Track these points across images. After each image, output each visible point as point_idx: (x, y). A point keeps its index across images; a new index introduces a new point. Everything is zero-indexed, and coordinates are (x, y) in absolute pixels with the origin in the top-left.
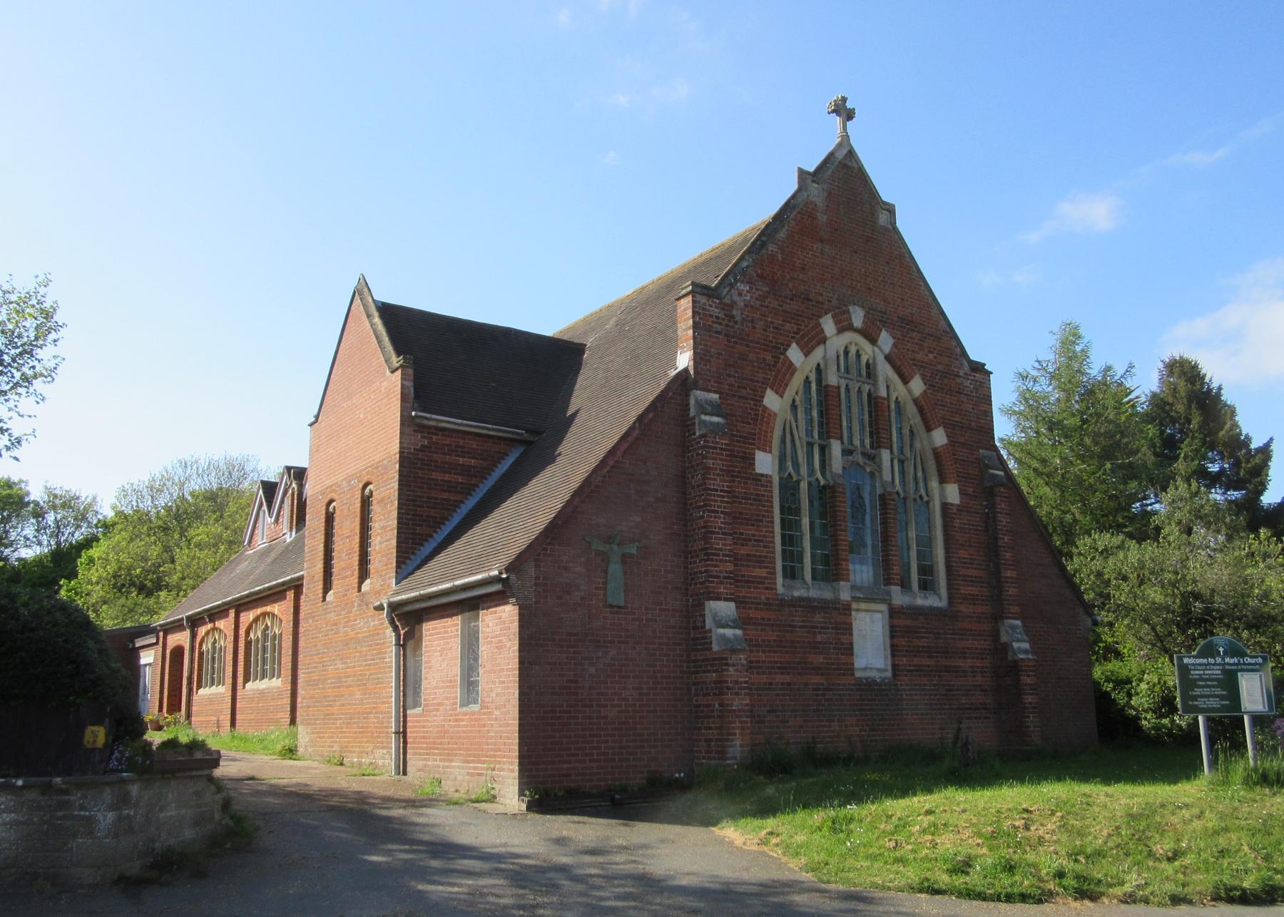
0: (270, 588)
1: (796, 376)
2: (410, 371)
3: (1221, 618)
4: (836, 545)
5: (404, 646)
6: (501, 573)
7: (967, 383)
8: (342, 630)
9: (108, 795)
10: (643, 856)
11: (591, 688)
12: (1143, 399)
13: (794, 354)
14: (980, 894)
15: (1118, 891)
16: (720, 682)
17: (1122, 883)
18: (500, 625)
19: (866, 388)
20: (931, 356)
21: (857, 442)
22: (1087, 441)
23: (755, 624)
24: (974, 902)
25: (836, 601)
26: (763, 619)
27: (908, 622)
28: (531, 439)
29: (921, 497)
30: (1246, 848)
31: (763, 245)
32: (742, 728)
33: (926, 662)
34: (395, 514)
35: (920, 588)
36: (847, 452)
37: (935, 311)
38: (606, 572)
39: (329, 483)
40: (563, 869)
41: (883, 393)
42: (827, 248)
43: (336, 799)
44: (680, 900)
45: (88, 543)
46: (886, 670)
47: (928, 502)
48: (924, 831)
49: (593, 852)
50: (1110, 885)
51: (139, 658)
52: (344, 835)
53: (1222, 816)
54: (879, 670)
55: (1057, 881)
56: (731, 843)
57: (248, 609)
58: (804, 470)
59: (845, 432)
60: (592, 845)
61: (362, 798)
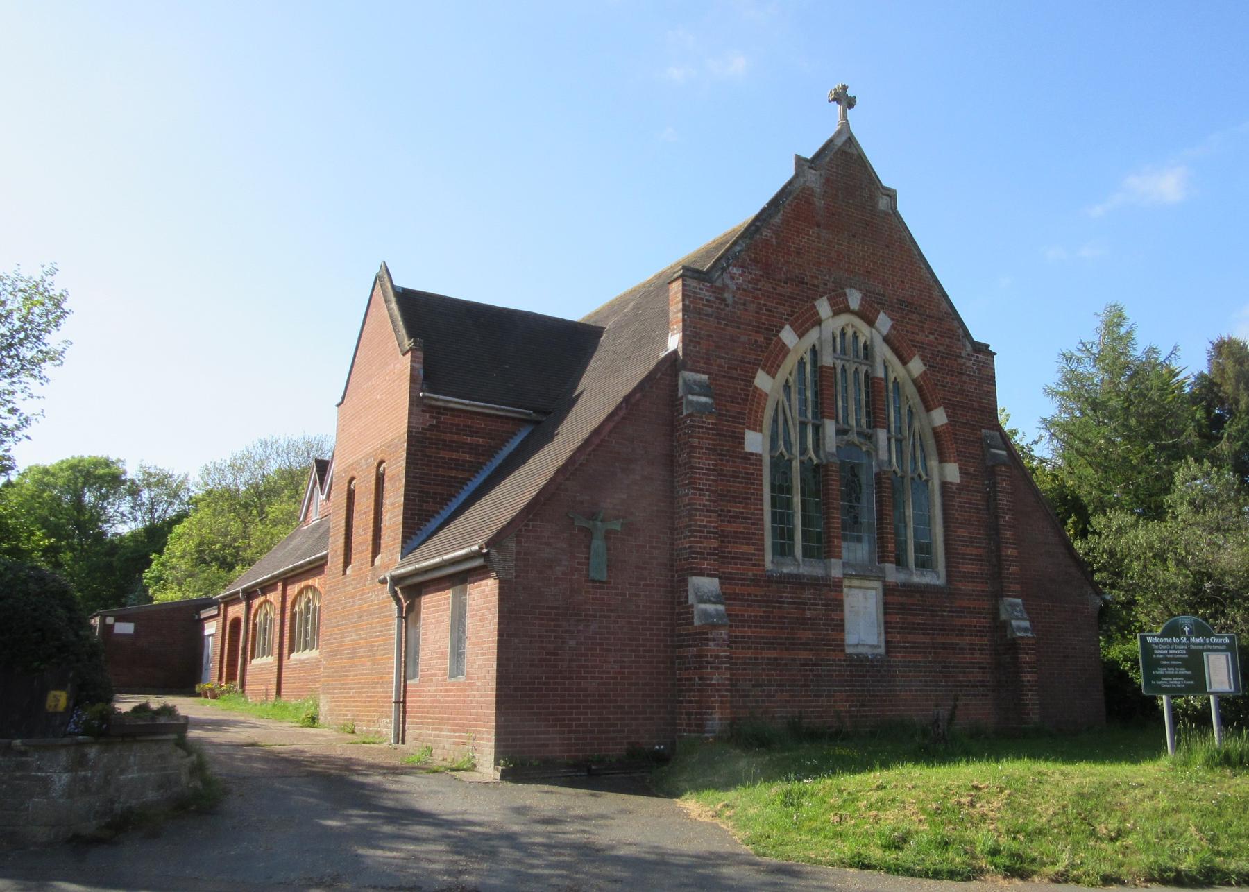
0: (310, 563)
1: (789, 357)
2: (420, 354)
3: (1232, 598)
4: (828, 523)
5: (406, 618)
6: (481, 548)
7: (970, 364)
8: (358, 603)
9: (63, 757)
10: (595, 826)
11: (571, 660)
12: (1192, 380)
13: (788, 336)
14: (908, 870)
15: (1050, 870)
16: (701, 656)
17: (1054, 863)
18: (483, 596)
19: (863, 369)
20: (931, 337)
21: (853, 422)
22: (1133, 422)
23: (741, 600)
24: (901, 878)
25: (827, 577)
26: (749, 595)
27: (903, 600)
28: (540, 418)
29: (920, 476)
30: (1193, 829)
31: (758, 230)
32: (721, 702)
33: (921, 639)
34: (402, 491)
35: (916, 566)
36: (840, 432)
37: (936, 294)
38: (589, 547)
39: (350, 461)
40: (511, 838)
41: (880, 373)
42: (824, 233)
43: (323, 765)
44: (610, 870)
45: (179, 519)
46: (878, 647)
47: (927, 481)
48: (870, 807)
49: (546, 821)
50: (1044, 864)
51: (203, 629)
52: (311, 800)
53: (1175, 796)
54: (872, 646)
55: (990, 858)
56: (687, 815)
57: (293, 583)
58: (796, 449)
59: (840, 412)
60: (550, 814)
61: (349, 765)
